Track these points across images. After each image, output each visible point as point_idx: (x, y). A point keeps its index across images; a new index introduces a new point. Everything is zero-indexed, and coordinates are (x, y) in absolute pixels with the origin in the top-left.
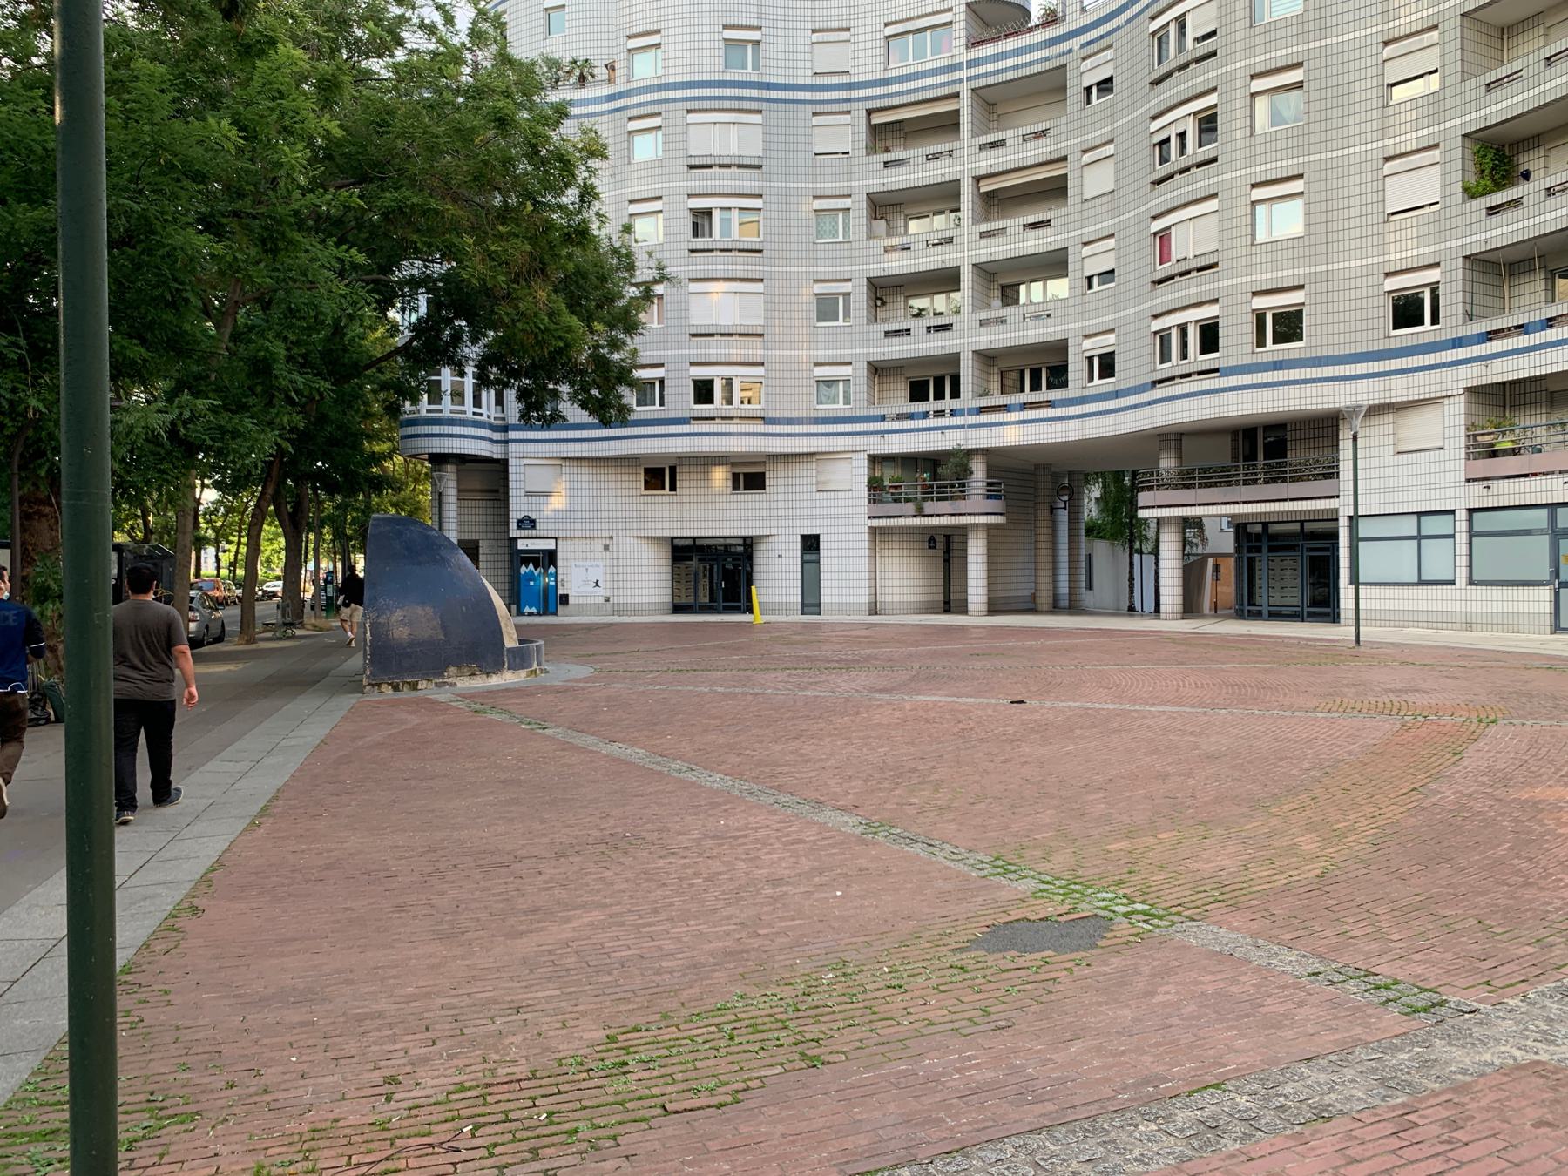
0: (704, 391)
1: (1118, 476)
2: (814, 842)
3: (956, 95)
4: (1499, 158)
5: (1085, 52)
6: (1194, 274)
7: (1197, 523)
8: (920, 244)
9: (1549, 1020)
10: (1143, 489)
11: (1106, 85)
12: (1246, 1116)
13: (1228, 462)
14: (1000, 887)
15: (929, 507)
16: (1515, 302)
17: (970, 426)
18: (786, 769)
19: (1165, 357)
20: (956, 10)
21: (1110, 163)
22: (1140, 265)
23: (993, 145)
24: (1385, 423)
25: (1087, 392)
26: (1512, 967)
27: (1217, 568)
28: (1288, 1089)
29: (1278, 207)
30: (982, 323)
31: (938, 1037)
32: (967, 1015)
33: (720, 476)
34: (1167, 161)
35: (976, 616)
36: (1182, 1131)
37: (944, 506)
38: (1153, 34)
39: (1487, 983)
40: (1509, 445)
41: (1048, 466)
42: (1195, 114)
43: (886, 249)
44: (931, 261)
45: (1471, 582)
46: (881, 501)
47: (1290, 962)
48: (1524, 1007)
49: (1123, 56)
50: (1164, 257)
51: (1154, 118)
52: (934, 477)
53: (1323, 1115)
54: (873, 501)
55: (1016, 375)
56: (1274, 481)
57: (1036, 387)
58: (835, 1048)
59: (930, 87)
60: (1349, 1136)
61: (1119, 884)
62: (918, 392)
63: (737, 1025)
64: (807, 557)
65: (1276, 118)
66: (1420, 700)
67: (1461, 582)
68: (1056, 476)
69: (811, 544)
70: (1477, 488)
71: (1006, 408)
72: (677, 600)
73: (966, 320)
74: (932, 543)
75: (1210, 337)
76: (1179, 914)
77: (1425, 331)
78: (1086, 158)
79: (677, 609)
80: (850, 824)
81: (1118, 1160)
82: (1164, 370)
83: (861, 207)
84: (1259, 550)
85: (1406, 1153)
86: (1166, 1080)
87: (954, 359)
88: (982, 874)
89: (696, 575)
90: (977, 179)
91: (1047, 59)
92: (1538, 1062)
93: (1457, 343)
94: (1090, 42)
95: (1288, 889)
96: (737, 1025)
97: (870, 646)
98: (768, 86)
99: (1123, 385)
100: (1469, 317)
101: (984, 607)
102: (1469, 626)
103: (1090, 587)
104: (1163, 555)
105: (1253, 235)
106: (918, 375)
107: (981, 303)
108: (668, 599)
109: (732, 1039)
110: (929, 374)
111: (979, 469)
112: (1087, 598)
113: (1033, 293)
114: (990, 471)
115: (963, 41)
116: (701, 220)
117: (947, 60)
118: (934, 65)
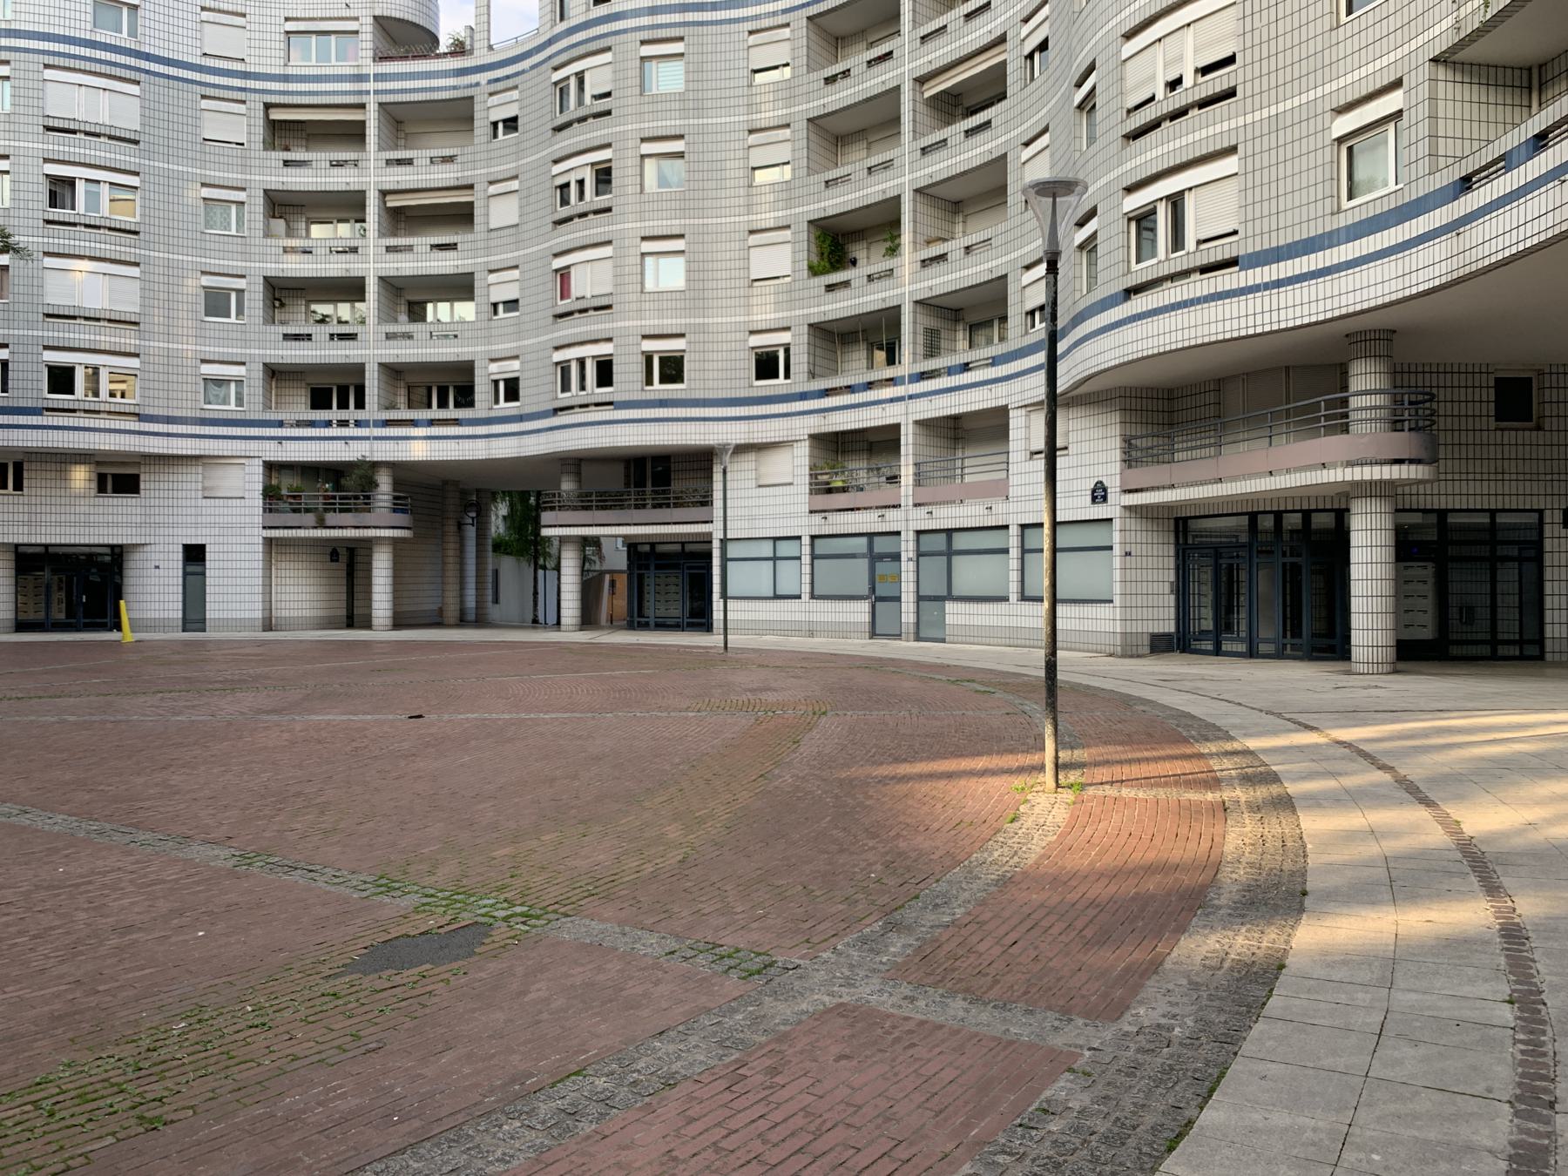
0: (61, 379)
1: (524, 495)
2: (176, 881)
3: (362, 106)
4: (836, 243)
5: (493, 88)
6: (591, 313)
7: (595, 542)
8: (322, 249)
9: (851, 967)
10: (545, 509)
11: (511, 124)
12: (602, 1096)
13: (620, 487)
14: (382, 905)
15: (331, 518)
16: (846, 366)
17: (376, 438)
18: (147, 804)
19: (566, 387)
20: (363, 20)
21: (514, 199)
22: (542, 299)
23: (400, 162)
24: (748, 462)
25: (493, 414)
26: (827, 924)
27: (613, 583)
28: (641, 1065)
29: (663, 261)
30: (389, 336)
31: (302, 1072)
32: (336, 1043)
33: (80, 476)
34: (568, 203)
35: (381, 630)
36: (543, 1122)
37: (347, 518)
38: (555, 84)
39: (808, 941)
40: (840, 484)
41: (456, 483)
42: (593, 164)
43: (285, 250)
44: (335, 268)
45: (813, 596)
46: (277, 511)
47: (651, 944)
48: (834, 958)
49: (527, 100)
50: (565, 294)
51: (556, 162)
52: (338, 487)
53: (670, 1083)
54: (268, 510)
55: (424, 391)
56: (660, 506)
57: (443, 404)
58: (180, 1104)
59: (334, 93)
60: (691, 1097)
61: (500, 889)
62: (320, 400)
63: (60, 1098)
64: (190, 569)
65: (662, 181)
66: (771, 697)
67: (806, 597)
68: (464, 493)
69: (194, 555)
70: (817, 518)
71: (413, 423)
72: (22, 617)
73: (373, 330)
74: (334, 556)
75: (605, 372)
76: (555, 912)
77: (779, 384)
78: (493, 189)
79: (21, 626)
80: (221, 857)
81: (480, 1164)
82: (564, 398)
83: (258, 205)
84: (647, 568)
85: (735, 1105)
86: (531, 1075)
87: (359, 369)
88: (365, 894)
89: (48, 587)
90: (384, 193)
91: (455, 88)
92: (842, 1004)
93: (803, 396)
94: (497, 80)
95: (654, 876)
96: (60, 1098)
97: (264, 660)
98: (148, 57)
99: (527, 410)
100: (812, 375)
101: (389, 622)
102: (811, 634)
103: (496, 601)
104: (563, 571)
105: (642, 283)
106: (322, 381)
107: (387, 315)
108: (11, 615)
109: (51, 1115)
110: (332, 382)
111: (384, 483)
112: (494, 612)
113: (439, 311)
114: (397, 484)
115: (370, 53)
116: (60, 191)
117: (346, 71)
118: (339, 71)
